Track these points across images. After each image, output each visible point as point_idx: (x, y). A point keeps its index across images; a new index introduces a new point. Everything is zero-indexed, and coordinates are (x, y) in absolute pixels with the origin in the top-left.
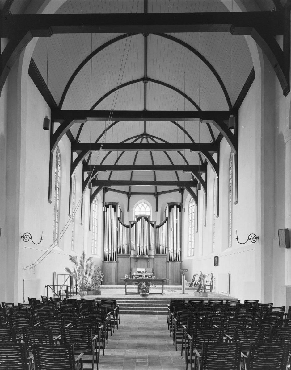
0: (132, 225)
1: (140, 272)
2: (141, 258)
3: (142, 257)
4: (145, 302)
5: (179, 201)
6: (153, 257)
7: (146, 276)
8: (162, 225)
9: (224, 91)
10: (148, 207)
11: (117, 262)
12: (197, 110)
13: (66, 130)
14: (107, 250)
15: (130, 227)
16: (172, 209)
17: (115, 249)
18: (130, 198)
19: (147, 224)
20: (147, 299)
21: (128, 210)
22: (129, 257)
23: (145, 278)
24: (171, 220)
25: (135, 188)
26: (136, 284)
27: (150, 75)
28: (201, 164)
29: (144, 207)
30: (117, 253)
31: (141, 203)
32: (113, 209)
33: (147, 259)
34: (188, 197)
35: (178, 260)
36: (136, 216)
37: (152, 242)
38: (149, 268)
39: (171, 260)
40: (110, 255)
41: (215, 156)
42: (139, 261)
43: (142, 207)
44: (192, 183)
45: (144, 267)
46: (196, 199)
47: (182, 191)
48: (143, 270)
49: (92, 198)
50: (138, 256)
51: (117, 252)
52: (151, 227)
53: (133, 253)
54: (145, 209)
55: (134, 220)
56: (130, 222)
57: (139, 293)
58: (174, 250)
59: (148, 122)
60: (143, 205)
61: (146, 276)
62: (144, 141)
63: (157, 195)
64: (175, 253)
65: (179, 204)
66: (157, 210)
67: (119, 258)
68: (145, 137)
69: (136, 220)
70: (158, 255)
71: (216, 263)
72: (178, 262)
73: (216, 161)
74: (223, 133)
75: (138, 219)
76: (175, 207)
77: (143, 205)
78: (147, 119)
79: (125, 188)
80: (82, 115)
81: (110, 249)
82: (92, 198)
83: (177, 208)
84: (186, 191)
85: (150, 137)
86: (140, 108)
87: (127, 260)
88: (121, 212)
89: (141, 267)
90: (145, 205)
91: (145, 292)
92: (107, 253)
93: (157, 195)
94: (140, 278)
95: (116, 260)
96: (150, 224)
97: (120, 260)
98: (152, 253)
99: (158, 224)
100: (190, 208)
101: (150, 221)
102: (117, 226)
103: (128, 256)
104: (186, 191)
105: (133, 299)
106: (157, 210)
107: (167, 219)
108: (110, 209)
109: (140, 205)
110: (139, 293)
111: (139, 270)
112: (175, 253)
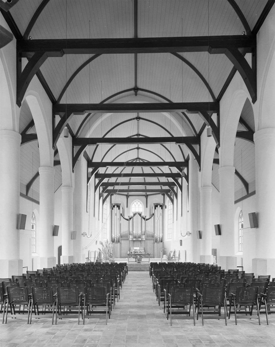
0: (130, 219)
1: (136, 250)
2: (137, 241)
3: (137, 240)
4: (139, 266)
5: (161, 202)
6: (144, 240)
7: (140, 252)
8: (150, 218)
9: (205, 84)
10: (141, 204)
11: (121, 243)
12: (171, 137)
13: (65, 124)
14: (114, 236)
15: (129, 220)
16: (157, 208)
17: (119, 234)
18: (129, 198)
19: (140, 217)
20: (140, 264)
21: (127, 207)
22: (128, 240)
23: (139, 253)
24: (156, 215)
25: (130, 193)
26: (133, 258)
27: (140, 86)
28: (184, 161)
29: (138, 204)
30: (120, 237)
31: (136, 202)
32: (118, 208)
33: (141, 241)
34: (167, 199)
35: (161, 242)
36: (133, 212)
37: (143, 230)
38: (141, 247)
39: (156, 242)
40: (116, 239)
41: (214, 117)
42: (135, 243)
43: (137, 206)
44: (170, 191)
45: (138, 247)
46: (172, 201)
47: (164, 195)
48: (138, 248)
49: (104, 201)
50: (134, 239)
51: (120, 236)
52: (143, 220)
53: (131, 237)
54: (139, 206)
55: (131, 215)
56: (129, 216)
57: (136, 261)
58: (158, 235)
59: (140, 55)
60: (137, 203)
61: (140, 252)
62: (138, 161)
63: (147, 196)
64: (159, 237)
65: (161, 204)
66: (147, 207)
67: (122, 241)
68: (138, 160)
69: (132, 215)
70: (148, 238)
71: (181, 244)
72: (161, 243)
73: (181, 184)
74: (207, 122)
75: (135, 215)
76: (159, 206)
77: (137, 203)
78: (139, 111)
79: (126, 193)
80: (94, 141)
81: (116, 234)
82: (104, 201)
83: (160, 207)
84: (166, 196)
85: (140, 159)
86: (129, 34)
87: (128, 241)
88: (122, 208)
89: (136, 247)
90: (139, 203)
91: (139, 261)
92: (114, 237)
93: (147, 196)
94: (136, 253)
95: (120, 242)
96: (142, 218)
97: (122, 242)
98: (143, 237)
99: (147, 218)
100: (169, 206)
101: (142, 216)
102: (120, 220)
103: (128, 240)
104: (166, 196)
105: (133, 264)
106: (147, 207)
107: (153, 215)
108: (116, 208)
109: (135, 203)
110: (136, 261)
111: (135, 248)
112: (159, 237)
